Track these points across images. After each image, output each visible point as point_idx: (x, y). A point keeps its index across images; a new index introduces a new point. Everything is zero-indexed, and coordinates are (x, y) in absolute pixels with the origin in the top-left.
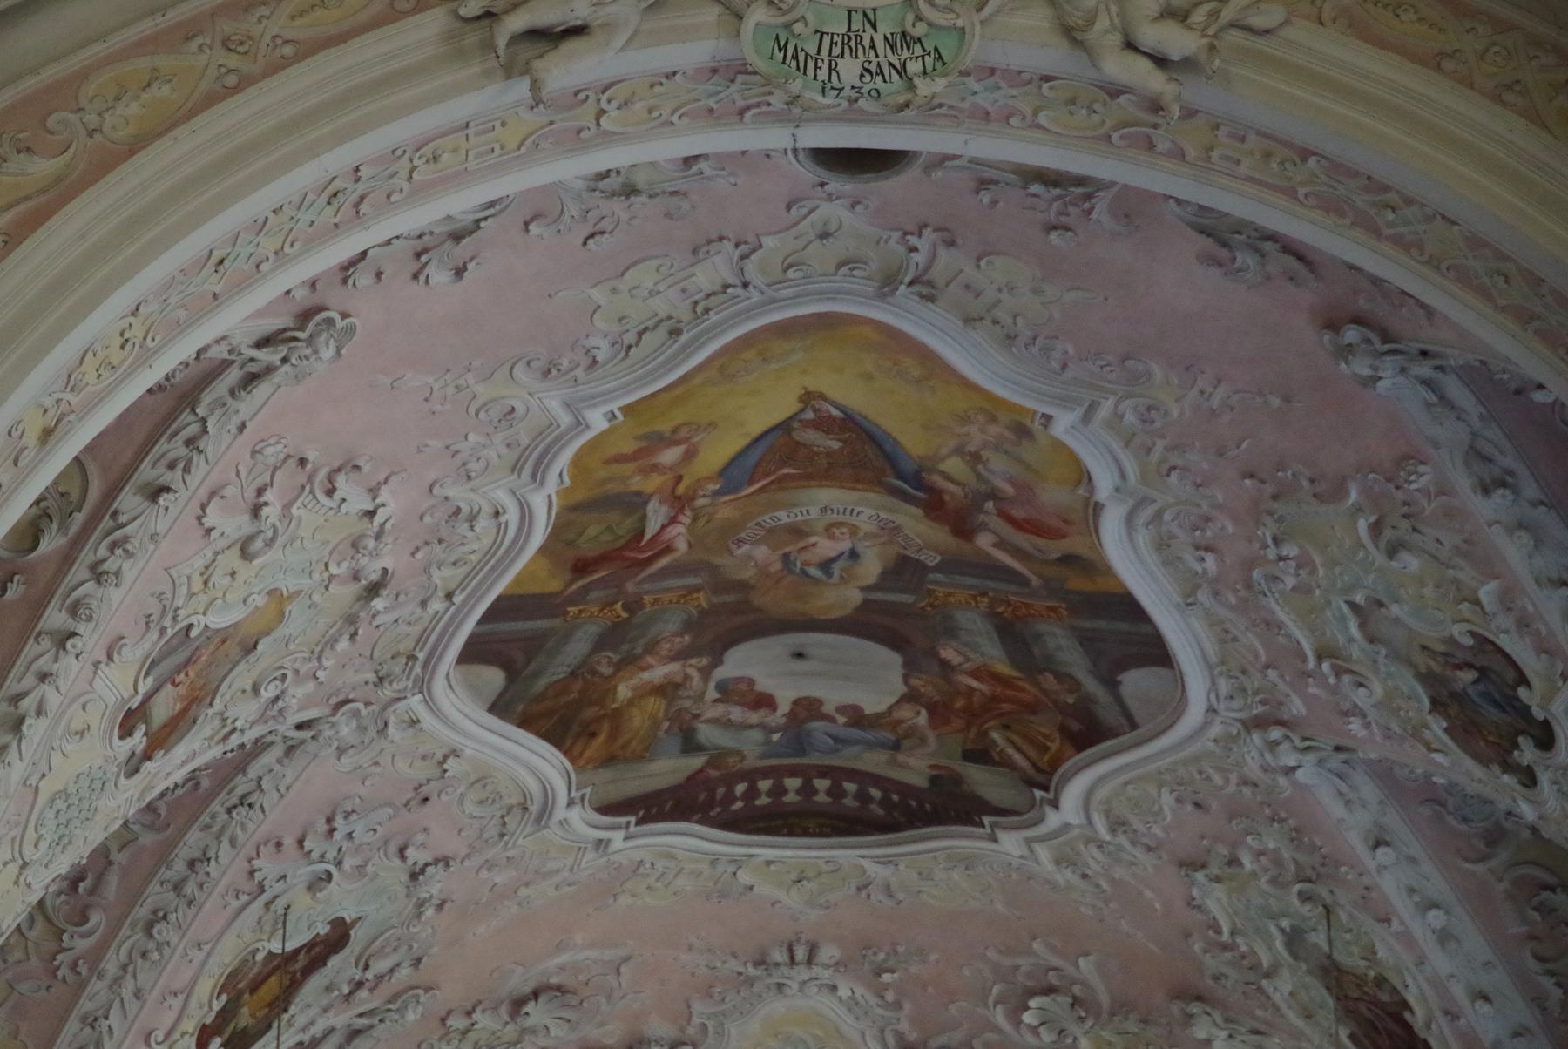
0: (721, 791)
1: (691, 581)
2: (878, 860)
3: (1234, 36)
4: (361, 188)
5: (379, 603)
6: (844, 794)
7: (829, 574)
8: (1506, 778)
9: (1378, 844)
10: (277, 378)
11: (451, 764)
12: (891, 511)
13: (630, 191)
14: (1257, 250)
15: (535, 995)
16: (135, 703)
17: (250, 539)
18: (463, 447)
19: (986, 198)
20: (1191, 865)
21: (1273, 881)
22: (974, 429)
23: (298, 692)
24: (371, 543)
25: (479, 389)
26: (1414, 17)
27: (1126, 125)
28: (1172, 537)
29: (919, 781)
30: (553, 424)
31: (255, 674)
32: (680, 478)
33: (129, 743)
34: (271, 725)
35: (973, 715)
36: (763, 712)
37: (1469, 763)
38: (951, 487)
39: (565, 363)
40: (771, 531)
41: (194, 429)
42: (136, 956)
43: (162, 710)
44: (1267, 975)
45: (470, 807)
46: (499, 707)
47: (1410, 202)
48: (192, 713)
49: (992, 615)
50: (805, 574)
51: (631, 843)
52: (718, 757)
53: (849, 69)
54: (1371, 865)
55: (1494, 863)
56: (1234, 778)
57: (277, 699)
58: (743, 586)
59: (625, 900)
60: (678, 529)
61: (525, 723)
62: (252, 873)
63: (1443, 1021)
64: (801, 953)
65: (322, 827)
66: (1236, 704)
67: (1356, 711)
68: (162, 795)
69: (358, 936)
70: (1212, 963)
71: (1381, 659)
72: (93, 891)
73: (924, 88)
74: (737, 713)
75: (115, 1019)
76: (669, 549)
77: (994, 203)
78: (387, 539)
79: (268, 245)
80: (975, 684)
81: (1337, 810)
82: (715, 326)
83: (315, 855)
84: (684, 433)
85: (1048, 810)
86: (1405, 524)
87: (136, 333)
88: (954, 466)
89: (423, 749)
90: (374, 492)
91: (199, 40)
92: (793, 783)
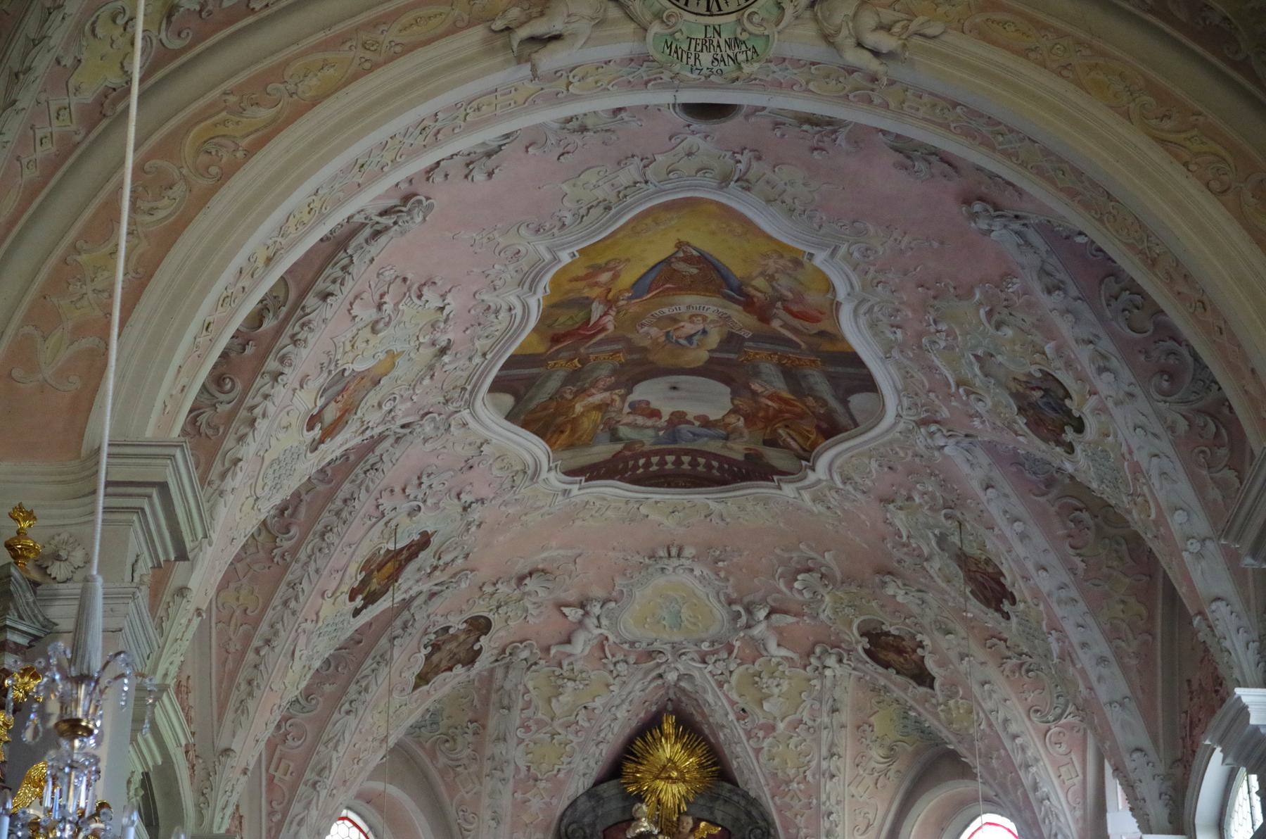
0: (631, 463)
1: (616, 347)
2: (716, 500)
3: (917, 40)
4: (438, 125)
5: (446, 359)
6: (698, 464)
7: (691, 343)
8: (1058, 449)
9: (988, 487)
10: (391, 232)
11: (484, 448)
12: (725, 307)
13: (583, 129)
14: (926, 160)
15: (531, 574)
16: (315, 412)
17: (377, 322)
18: (492, 272)
19: (778, 133)
20: (886, 501)
21: (931, 508)
22: (771, 262)
23: (402, 408)
24: (442, 325)
25: (500, 240)
26: (1013, 29)
27: (857, 89)
28: (878, 320)
29: (740, 457)
30: (541, 260)
31: (379, 397)
32: (609, 290)
33: (312, 434)
34: (388, 426)
35: (770, 420)
36: (654, 419)
37: (1038, 441)
38: (759, 295)
39: (548, 226)
40: (660, 319)
41: (346, 261)
42: (316, 551)
43: (330, 415)
44: (927, 560)
45: (496, 472)
46: (511, 417)
47: (1011, 131)
48: (345, 419)
49: (779, 364)
50: (677, 342)
51: (581, 491)
52: (630, 444)
53: (706, 58)
54: (984, 499)
55: (1050, 496)
56: (910, 453)
57: (391, 411)
58: (644, 349)
59: (578, 523)
60: (609, 318)
61: (525, 425)
62: (378, 507)
63: (1021, 582)
64: (674, 551)
65: (416, 482)
66: (911, 412)
67: (978, 415)
68: (329, 463)
69: (435, 541)
70: (898, 554)
71: (991, 386)
72: (292, 515)
73: (747, 69)
74: (640, 420)
75: (305, 584)
76: (604, 329)
77: (783, 135)
78: (451, 323)
79: (388, 156)
80: (770, 403)
81: (966, 469)
82: (631, 204)
83: (411, 497)
84: (612, 265)
85: (810, 472)
86: (1006, 311)
87: (316, 205)
88: (760, 282)
89: (469, 440)
90: (443, 297)
91: (349, 44)
92: (670, 458)
